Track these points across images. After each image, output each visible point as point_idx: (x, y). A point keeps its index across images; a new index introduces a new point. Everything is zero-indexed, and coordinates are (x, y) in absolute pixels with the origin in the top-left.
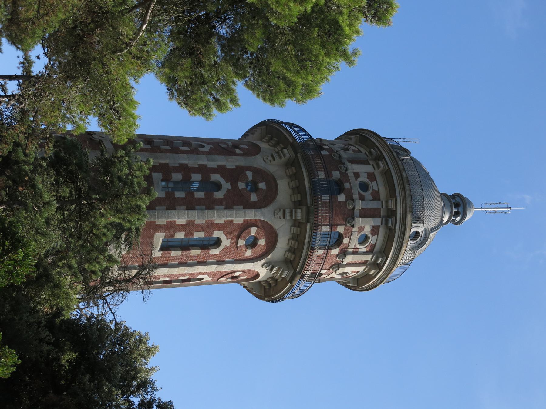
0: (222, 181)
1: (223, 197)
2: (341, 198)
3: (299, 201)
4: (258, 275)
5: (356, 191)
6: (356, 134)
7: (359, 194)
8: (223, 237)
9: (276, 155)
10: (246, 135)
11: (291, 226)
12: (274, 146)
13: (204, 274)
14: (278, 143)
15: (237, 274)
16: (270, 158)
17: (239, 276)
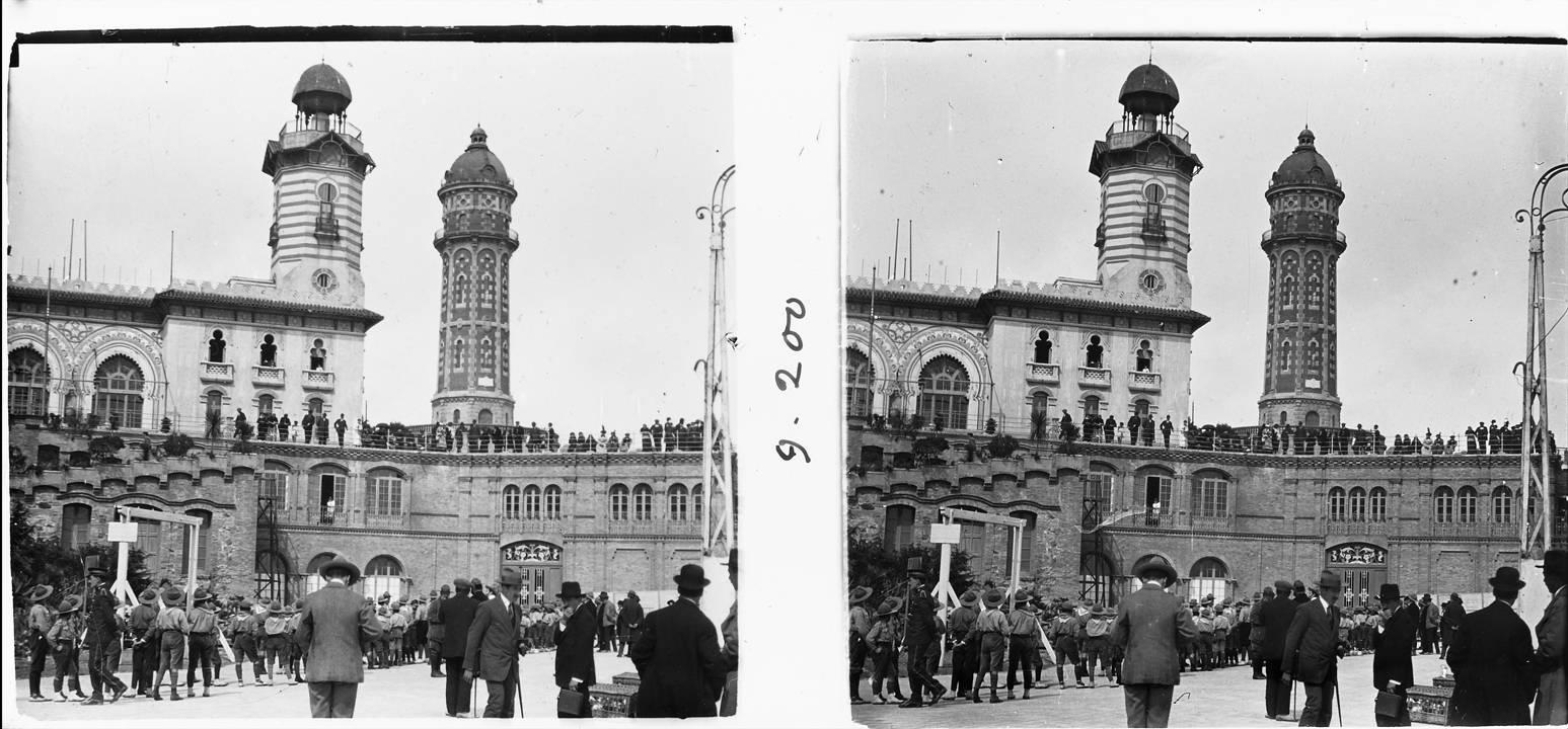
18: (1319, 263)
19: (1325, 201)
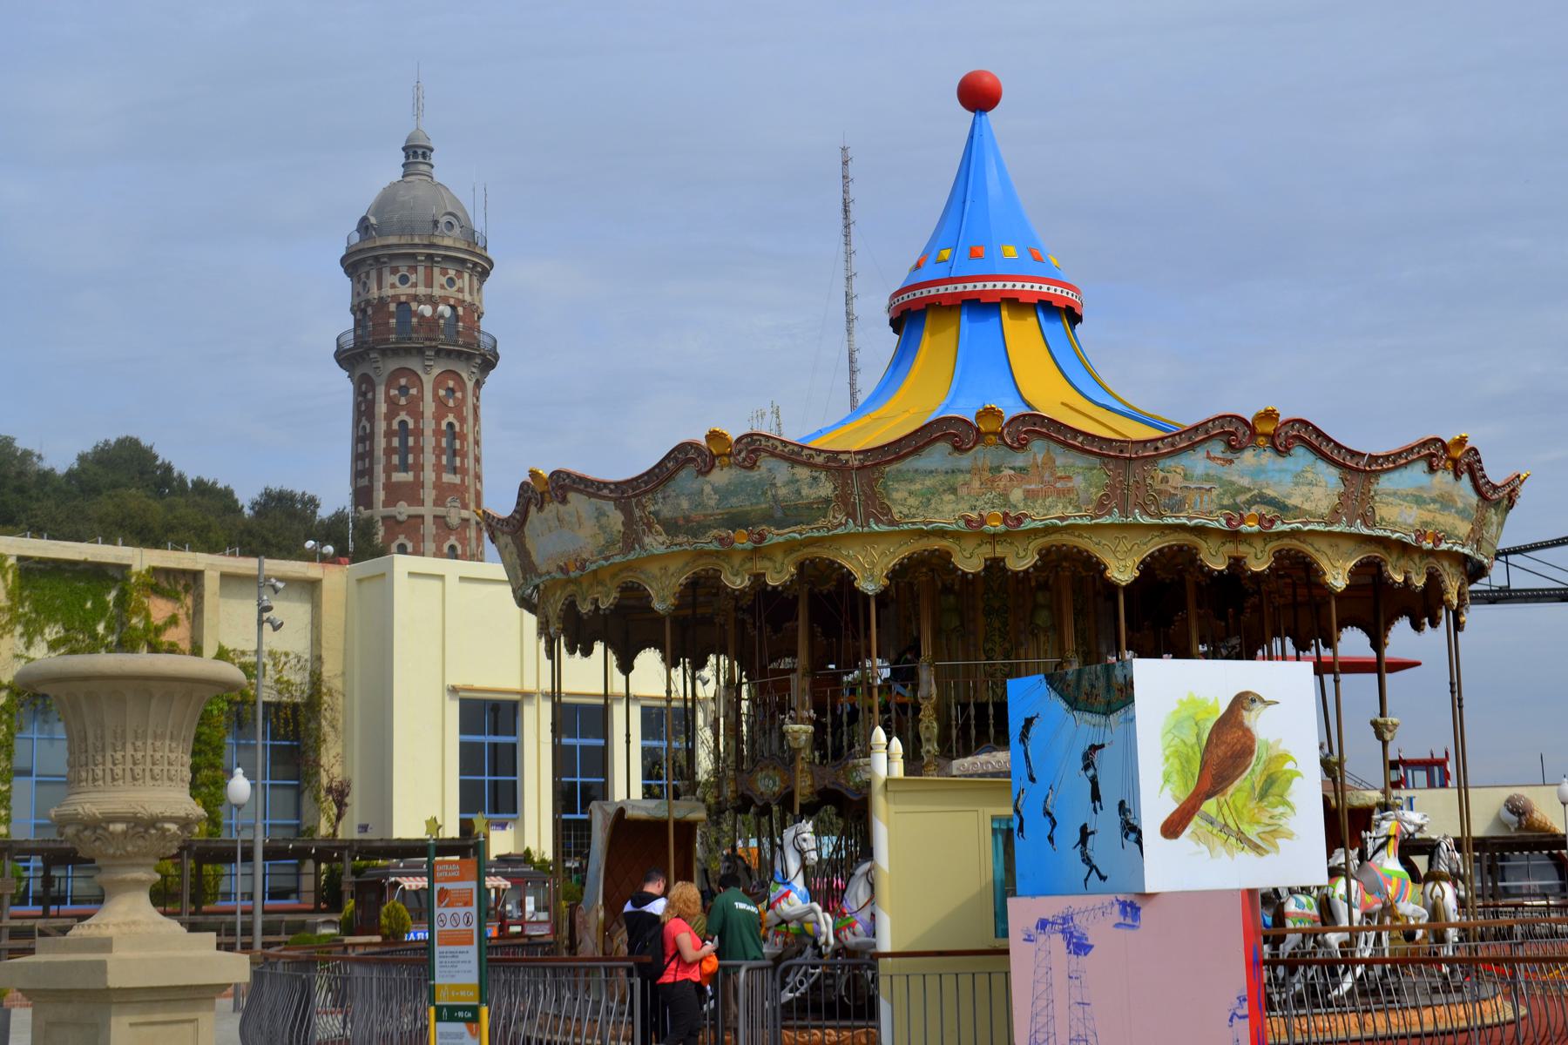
18: (394, 392)
19: (421, 270)
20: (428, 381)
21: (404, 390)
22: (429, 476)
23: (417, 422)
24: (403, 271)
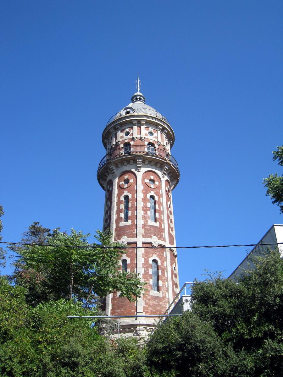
0: (124, 195)
1: (130, 259)
2: (132, 143)
3: (133, 161)
4: (167, 181)
5: (129, 137)
6: (104, 141)
7: (131, 135)
8: (153, 258)
9: (112, 172)
10: (103, 188)
11: (145, 164)
12: (109, 174)
13: (167, 204)
14: (107, 172)
15: (167, 190)
16: (114, 175)
17: (168, 189)
20: (140, 175)
21: (127, 181)
22: (140, 222)
23: (133, 195)
24: (127, 130)
